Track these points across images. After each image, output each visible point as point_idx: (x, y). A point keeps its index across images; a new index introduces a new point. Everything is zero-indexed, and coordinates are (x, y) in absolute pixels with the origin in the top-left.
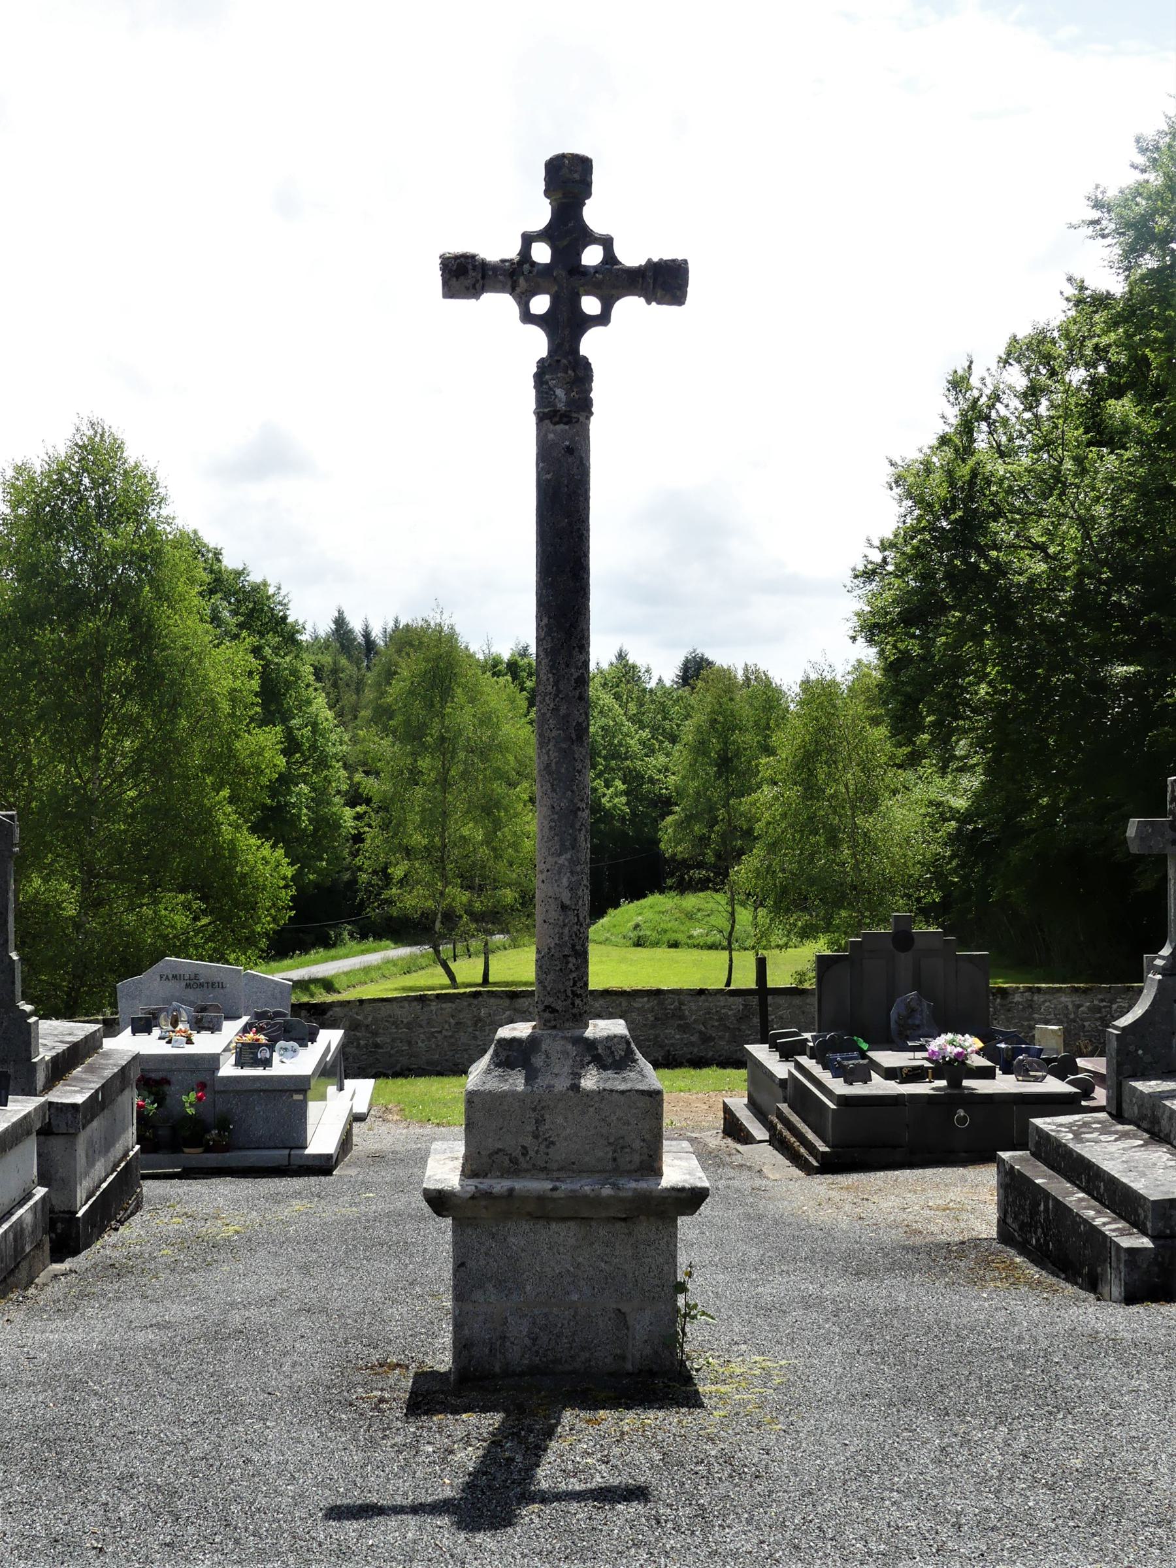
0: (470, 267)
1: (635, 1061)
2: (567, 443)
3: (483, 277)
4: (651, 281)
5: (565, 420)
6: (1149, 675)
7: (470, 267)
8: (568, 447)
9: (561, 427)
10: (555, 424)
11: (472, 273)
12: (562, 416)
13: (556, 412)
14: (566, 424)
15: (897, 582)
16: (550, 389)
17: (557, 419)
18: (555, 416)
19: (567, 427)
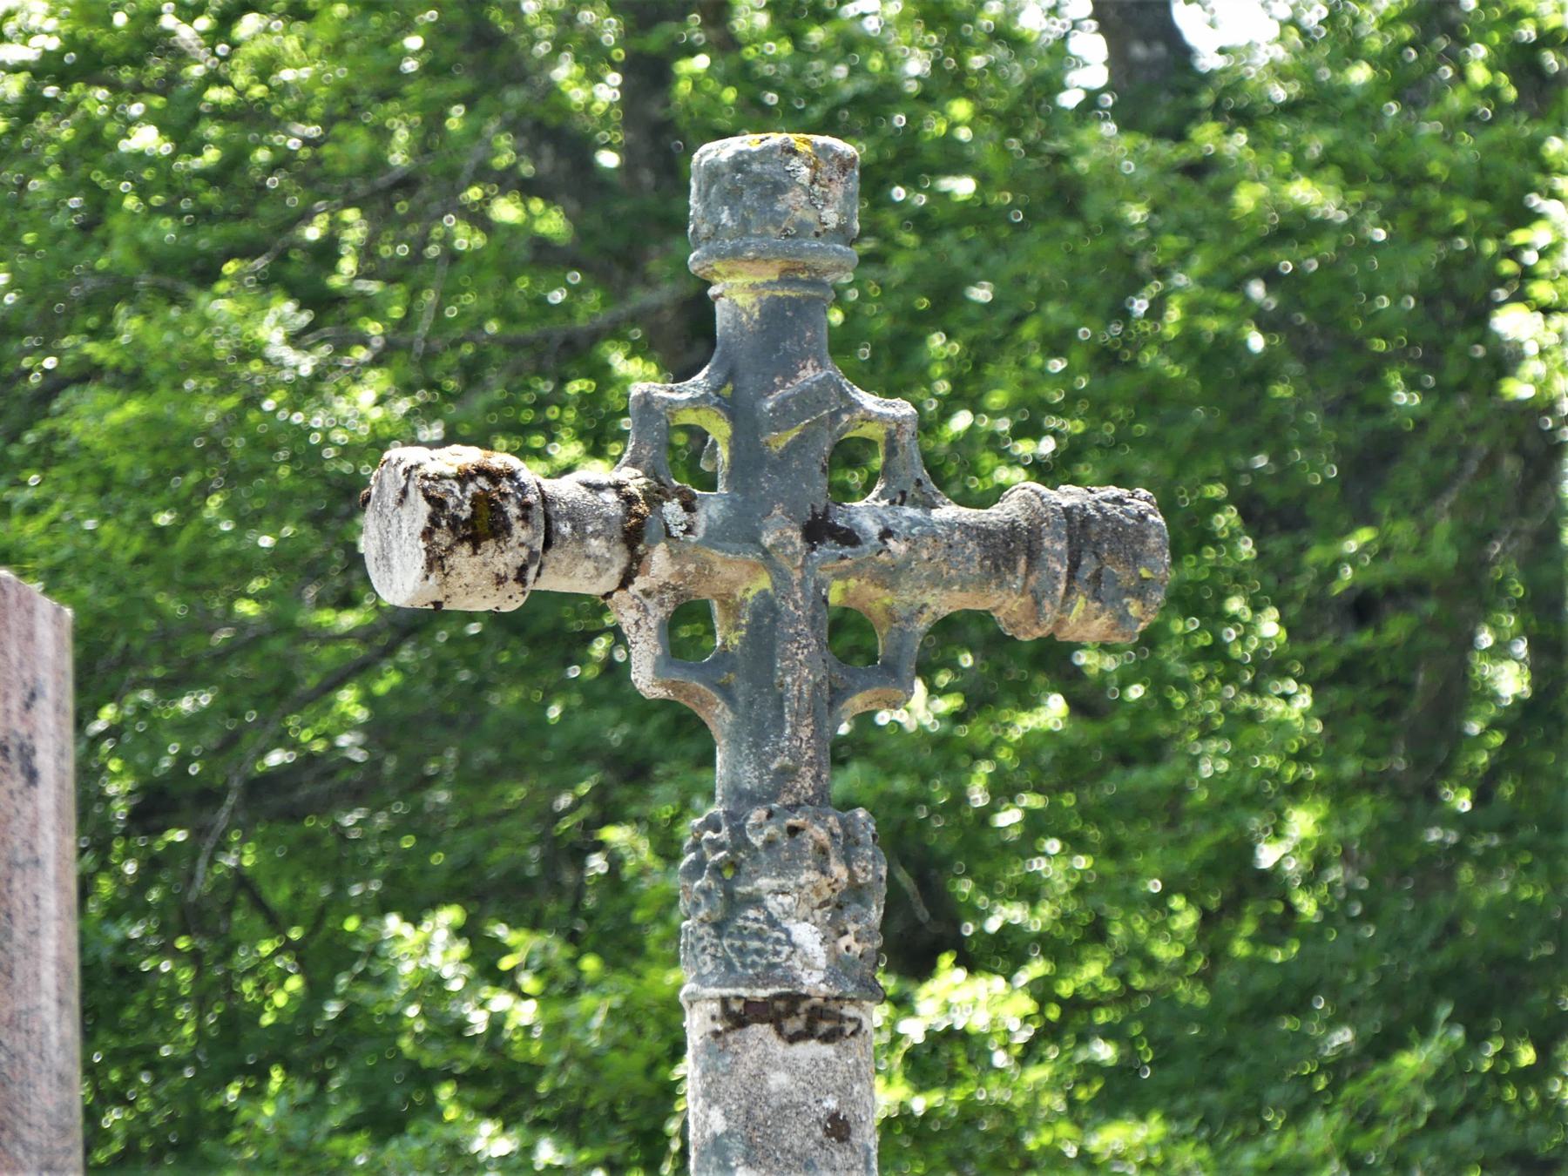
0: (513, 510)
1: (707, 528)
2: (831, 1103)
3: (548, 544)
4: (1062, 570)
5: (824, 1026)
6: (1102, 878)
7: (513, 510)
8: (834, 1117)
9: (810, 1050)
10: (793, 1039)
11: (519, 532)
12: (817, 1014)
13: (794, 1000)
14: (827, 1038)
15: (1244, 1046)
16: (773, 923)
17: (795, 1024)
18: (791, 1012)
19: (828, 1050)
